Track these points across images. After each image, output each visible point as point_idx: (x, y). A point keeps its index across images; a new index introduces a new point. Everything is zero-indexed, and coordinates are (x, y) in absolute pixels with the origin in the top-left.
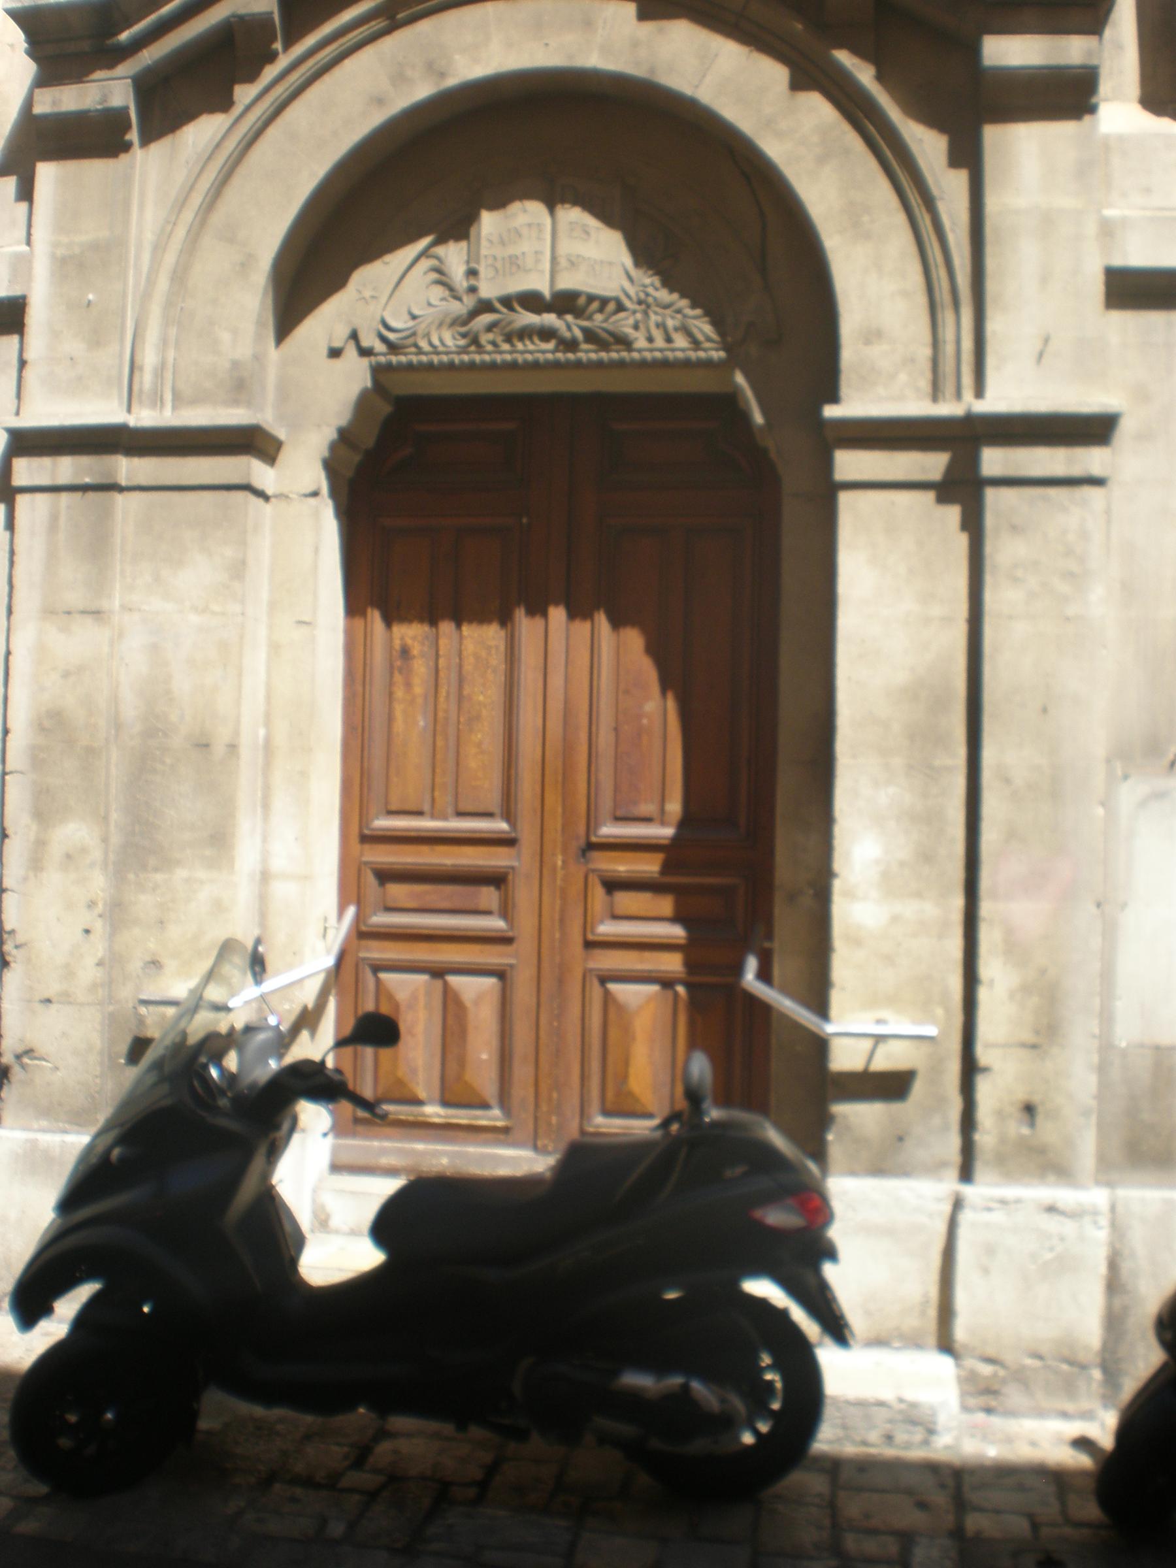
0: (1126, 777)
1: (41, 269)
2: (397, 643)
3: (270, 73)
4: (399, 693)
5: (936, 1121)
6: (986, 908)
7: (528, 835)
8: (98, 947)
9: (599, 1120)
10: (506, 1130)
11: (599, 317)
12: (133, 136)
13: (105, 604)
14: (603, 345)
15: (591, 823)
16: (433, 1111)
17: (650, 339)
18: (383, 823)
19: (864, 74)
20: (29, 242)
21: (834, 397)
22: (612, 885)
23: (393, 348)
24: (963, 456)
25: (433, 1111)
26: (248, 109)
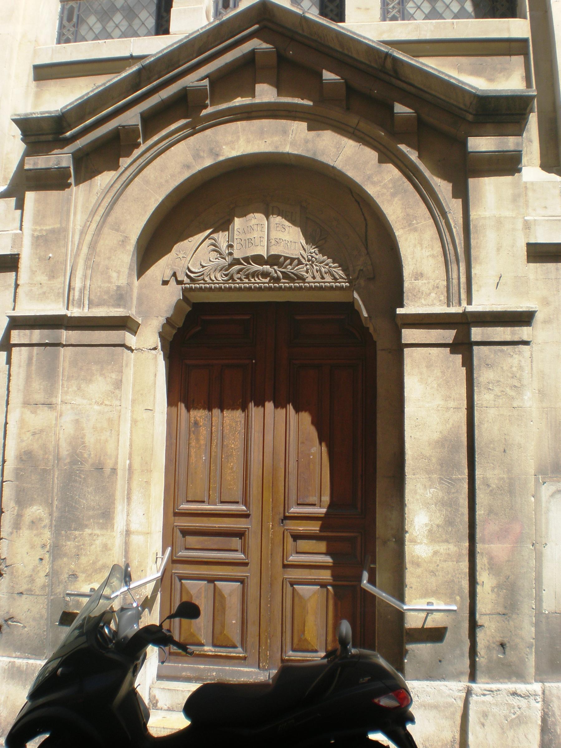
0: (544, 483)
1: (27, 241)
2: (192, 420)
3: (137, 152)
4: (193, 443)
5: (458, 652)
6: (479, 547)
7: (255, 512)
8: (46, 567)
9: (291, 653)
10: (245, 658)
11: (289, 267)
12: (72, 180)
13: (54, 400)
14: (292, 280)
15: (286, 507)
16: (208, 649)
17: (314, 277)
18: (185, 506)
19: (413, 156)
20: (21, 229)
22: (296, 537)
23: (192, 280)
24: (463, 332)
25: (208, 649)
26: (126, 169)
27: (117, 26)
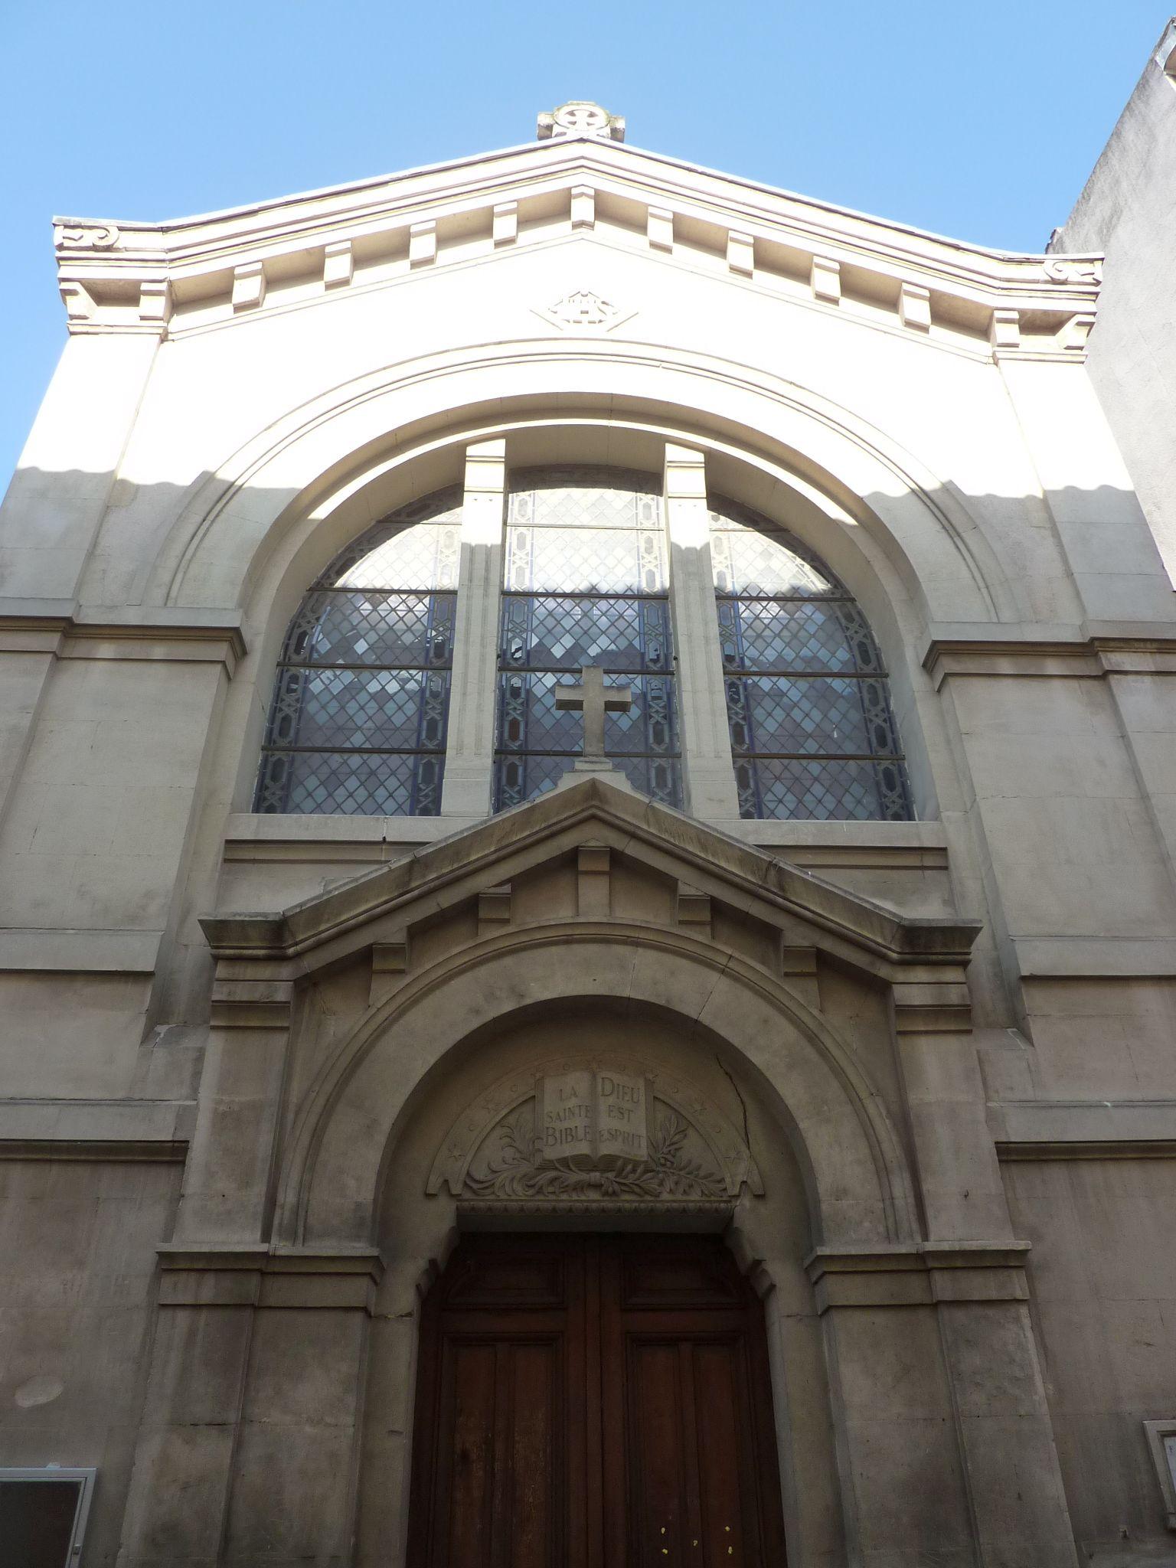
21: (821, 1242)
27: (351, 795)
